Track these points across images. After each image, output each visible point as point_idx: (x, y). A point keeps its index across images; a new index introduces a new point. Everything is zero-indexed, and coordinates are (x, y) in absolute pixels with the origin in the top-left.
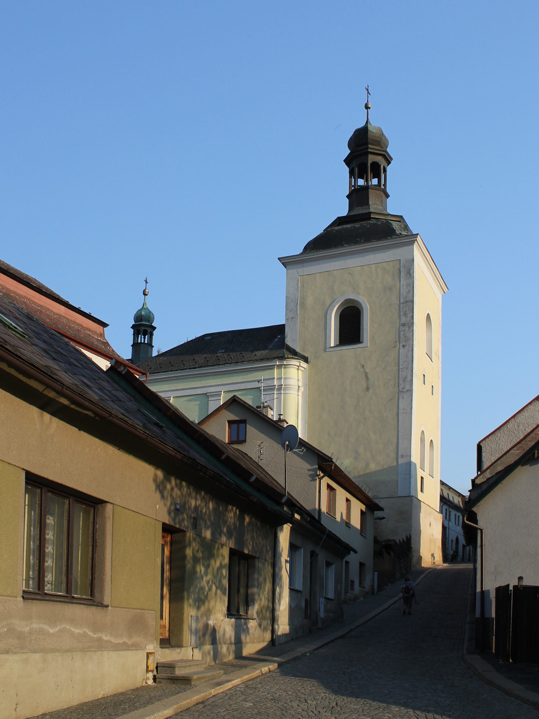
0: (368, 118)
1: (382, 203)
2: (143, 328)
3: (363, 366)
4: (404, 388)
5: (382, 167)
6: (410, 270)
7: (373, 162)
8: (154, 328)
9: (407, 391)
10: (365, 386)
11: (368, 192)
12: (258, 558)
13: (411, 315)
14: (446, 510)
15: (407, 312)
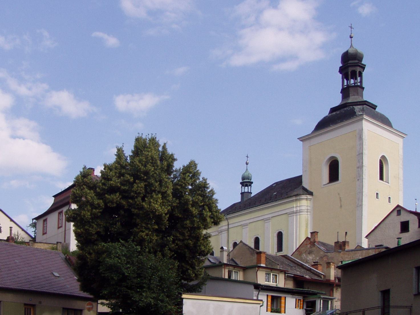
0: (351, 44)
2: (245, 184)
3: (339, 194)
4: (358, 204)
6: (361, 135)
8: (252, 183)
10: (340, 205)
12: (84, 310)
13: (362, 161)
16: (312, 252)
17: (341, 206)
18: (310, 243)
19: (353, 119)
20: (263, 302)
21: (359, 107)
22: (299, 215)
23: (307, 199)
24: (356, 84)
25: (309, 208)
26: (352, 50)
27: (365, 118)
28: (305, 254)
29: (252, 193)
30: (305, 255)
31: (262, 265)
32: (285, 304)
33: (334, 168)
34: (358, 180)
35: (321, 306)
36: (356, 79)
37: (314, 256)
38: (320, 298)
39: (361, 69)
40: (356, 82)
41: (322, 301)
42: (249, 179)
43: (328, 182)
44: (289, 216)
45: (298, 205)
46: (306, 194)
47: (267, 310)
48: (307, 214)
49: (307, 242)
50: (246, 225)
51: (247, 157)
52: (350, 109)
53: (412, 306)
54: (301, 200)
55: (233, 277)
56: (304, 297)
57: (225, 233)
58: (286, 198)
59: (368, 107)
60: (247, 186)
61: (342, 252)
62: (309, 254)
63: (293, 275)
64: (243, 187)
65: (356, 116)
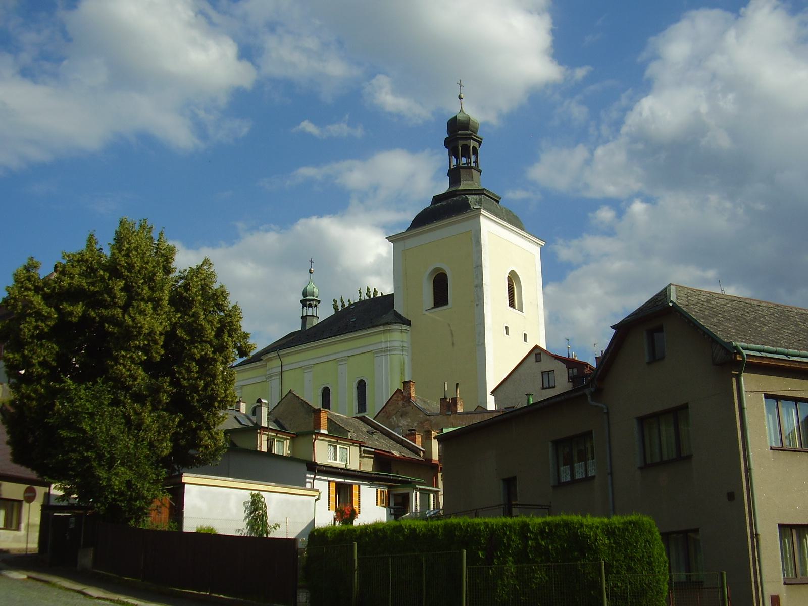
2: (308, 303)
16: (407, 413)
17: (453, 344)
18: (403, 399)
19: (466, 214)
20: (319, 494)
21: (474, 197)
22: (390, 355)
23: (402, 331)
24: (469, 165)
25: (405, 345)
26: (462, 116)
27: (484, 214)
28: (396, 417)
29: (318, 318)
30: (395, 419)
31: (322, 431)
32: (359, 498)
33: (440, 285)
34: (477, 305)
35: (418, 504)
36: (469, 157)
37: (409, 420)
38: (415, 488)
39: (477, 145)
40: (469, 161)
41: (418, 493)
42: (313, 296)
43: (433, 306)
44: (375, 355)
45: (389, 340)
46: (400, 323)
47: (329, 507)
48: (402, 353)
49: (398, 397)
50: (310, 367)
51: (312, 261)
52: (462, 200)
53: (550, 506)
54: (392, 332)
55: (276, 451)
56: (389, 487)
57: (277, 379)
58: (369, 328)
59: (488, 198)
60: (312, 307)
61: (452, 415)
62: (402, 416)
63: (373, 450)
64: (305, 307)
65: (471, 209)
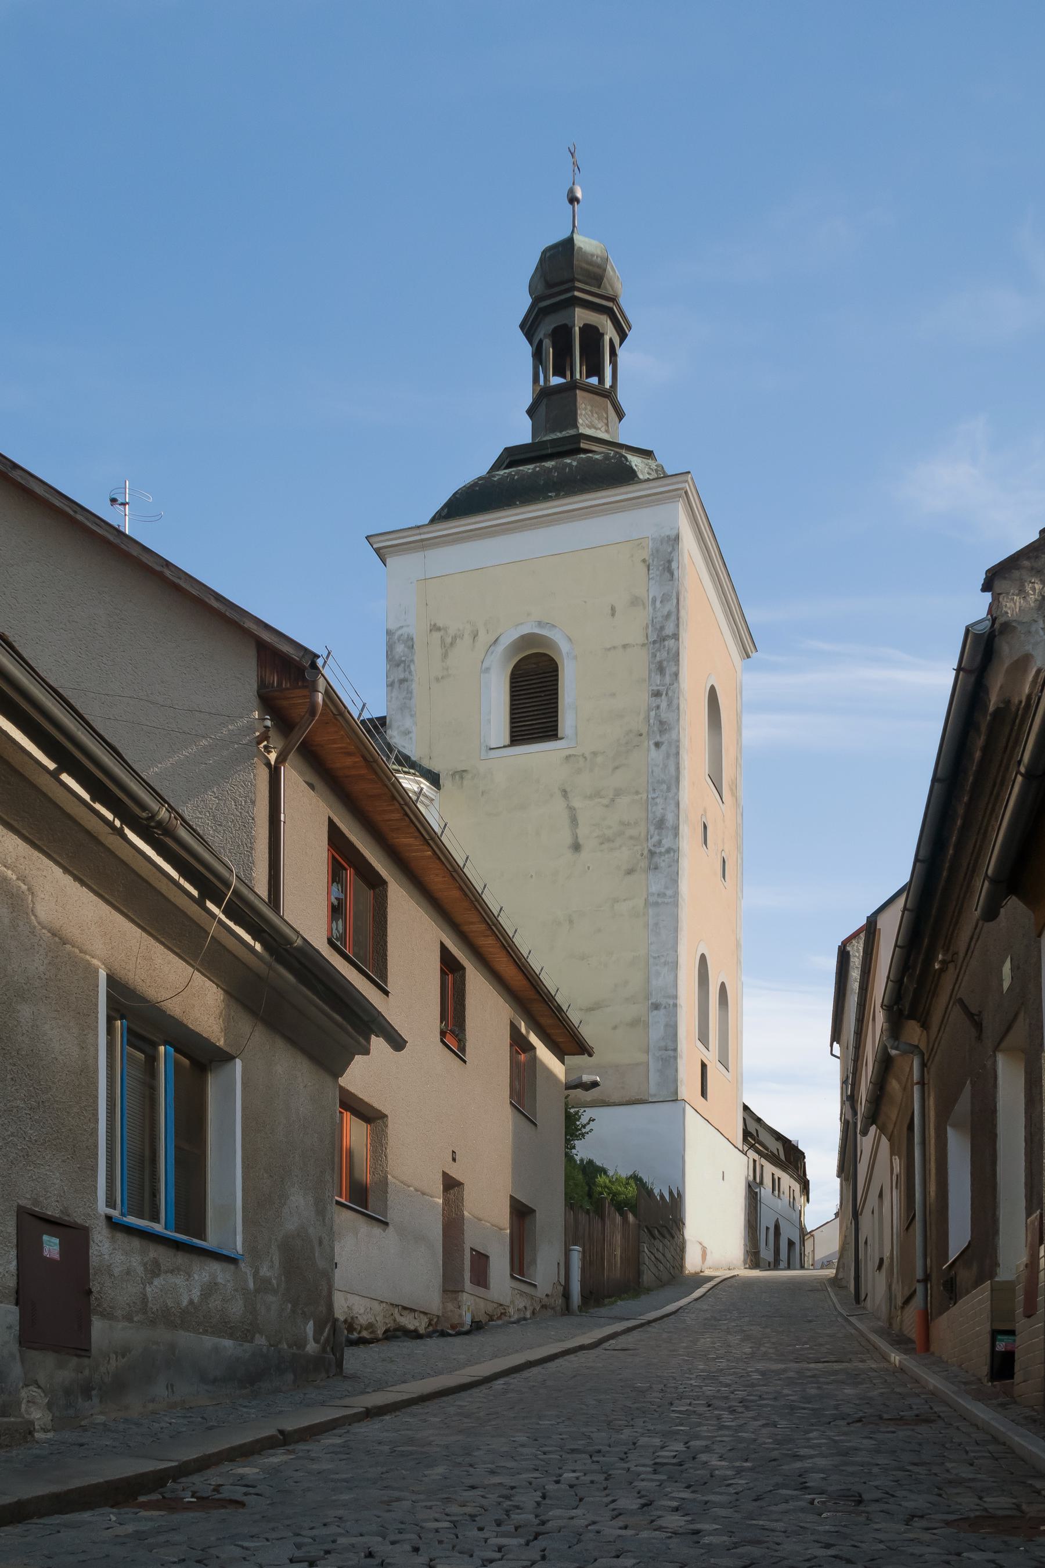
1: (607, 425)
5: (607, 338)
6: (670, 562)
7: (585, 325)
9: (668, 851)
11: (576, 395)
14: (755, 1161)
15: (665, 664)
